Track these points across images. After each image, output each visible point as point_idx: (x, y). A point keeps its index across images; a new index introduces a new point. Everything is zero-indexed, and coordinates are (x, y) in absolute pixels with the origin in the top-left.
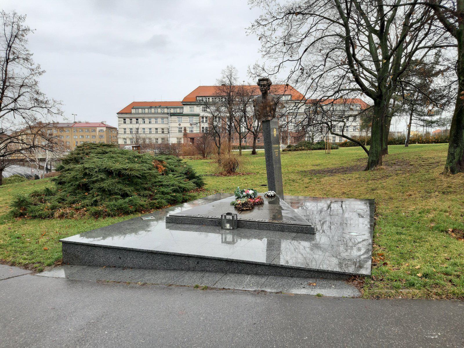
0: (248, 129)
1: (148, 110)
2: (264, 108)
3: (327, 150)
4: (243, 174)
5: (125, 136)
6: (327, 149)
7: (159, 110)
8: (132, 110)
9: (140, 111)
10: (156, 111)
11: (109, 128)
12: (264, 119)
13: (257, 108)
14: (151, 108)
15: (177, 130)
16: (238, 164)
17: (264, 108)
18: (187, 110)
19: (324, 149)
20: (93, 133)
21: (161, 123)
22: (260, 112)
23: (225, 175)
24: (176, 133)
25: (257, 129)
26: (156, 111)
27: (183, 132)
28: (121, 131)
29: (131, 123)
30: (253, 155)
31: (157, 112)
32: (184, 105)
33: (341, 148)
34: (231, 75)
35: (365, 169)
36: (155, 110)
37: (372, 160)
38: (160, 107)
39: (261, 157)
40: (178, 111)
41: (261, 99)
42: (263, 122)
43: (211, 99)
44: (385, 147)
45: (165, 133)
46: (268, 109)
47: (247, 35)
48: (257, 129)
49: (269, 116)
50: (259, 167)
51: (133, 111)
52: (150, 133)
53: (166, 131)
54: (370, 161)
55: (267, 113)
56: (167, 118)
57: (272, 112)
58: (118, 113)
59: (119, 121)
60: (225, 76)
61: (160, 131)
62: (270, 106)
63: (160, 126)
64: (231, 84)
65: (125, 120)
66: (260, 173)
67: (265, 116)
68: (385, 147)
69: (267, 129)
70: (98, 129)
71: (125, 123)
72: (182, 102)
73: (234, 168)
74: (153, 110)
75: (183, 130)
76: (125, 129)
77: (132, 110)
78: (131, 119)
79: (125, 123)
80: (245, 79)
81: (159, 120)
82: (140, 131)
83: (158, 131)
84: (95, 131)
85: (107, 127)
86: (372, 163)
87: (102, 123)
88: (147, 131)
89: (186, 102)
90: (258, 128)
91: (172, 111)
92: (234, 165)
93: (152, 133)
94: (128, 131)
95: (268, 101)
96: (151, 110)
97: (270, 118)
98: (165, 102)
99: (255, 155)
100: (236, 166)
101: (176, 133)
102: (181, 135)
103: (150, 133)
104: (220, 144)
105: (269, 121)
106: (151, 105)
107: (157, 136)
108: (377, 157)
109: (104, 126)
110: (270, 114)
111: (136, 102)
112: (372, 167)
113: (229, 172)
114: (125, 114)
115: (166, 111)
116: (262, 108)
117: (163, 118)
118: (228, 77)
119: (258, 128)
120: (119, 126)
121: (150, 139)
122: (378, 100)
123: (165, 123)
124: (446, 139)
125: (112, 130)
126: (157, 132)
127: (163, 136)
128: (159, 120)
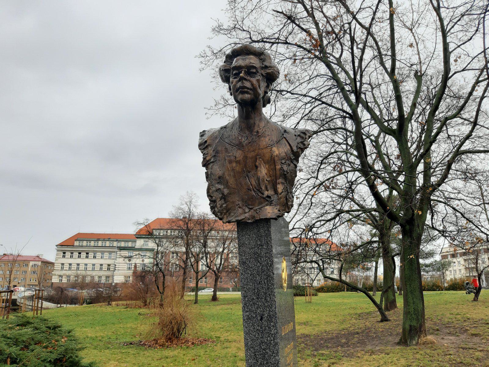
0: (208, 267)
1: (95, 243)
2: (248, 167)
3: (307, 297)
4: (193, 343)
5: (62, 273)
6: (307, 295)
7: (108, 244)
8: (75, 242)
9: (85, 243)
10: (104, 244)
11: (46, 263)
12: (245, 215)
13: (217, 170)
14: (98, 240)
15: (126, 267)
16: (186, 325)
17: (248, 167)
18: (140, 243)
19: (304, 295)
20: (24, 268)
21: (108, 258)
22: (232, 181)
23: (162, 346)
24: (125, 270)
25: (219, 267)
26: (104, 244)
27: (133, 269)
28: (58, 266)
29: (79, 257)
30: (213, 303)
31: (105, 245)
32: (137, 238)
33: (321, 294)
34: (191, 202)
35: (397, 340)
36: (103, 243)
37: (410, 326)
38: (109, 240)
39: (224, 306)
40: (130, 244)
41: (235, 132)
42: (241, 225)
43: (169, 231)
44: (393, 298)
45: (111, 269)
46: (263, 171)
47: (208, 118)
48: (219, 267)
49: (268, 200)
50: (220, 326)
51: (76, 243)
52: (93, 269)
53: (112, 268)
54: (407, 327)
55: (260, 190)
56: (116, 252)
57: (280, 188)
58: (57, 246)
59: (57, 255)
60: (184, 202)
61: (105, 267)
62: (272, 161)
63: (105, 262)
64: (190, 212)
65: (64, 253)
66: (222, 339)
67: (249, 202)
68: (393, 298)
69: (257, 257)
70: (31, 263)
71: (64, 257)
72: (136, 235)
73: (179, 331)
74: (100, 243)
75: (133, 266)
76: (63, 264)
77: (75, 242)
78: (72, 253)
79: (64, 257)
80: (199, 157)
81: (106, 255)
82: (82, 267)
83: (103, 267)
84: (27, 265)
85: (42, 262)
86: (410, 330)
87: (37, 256)
88: (90, 267)
89: (139, 236)
90: (220, 266)
91: (123, 244)
92: (179, 325)
93: (96, 269)
94: (66, 267)
95: (265, 141)
96: (98, 243)
97: (270, 211)
98: (116, 234)
99: (216, 303)
100: (183, 326)
101: (125, 270)
102: (130, 273)
103: (93, 269)
104: (164, 288)
105: (267, 221)
106: (98, 237)
107: (101, 273)
108: (418, 320)
109: (39, 260)
110: (270, 192)
111: (81, 233)
112: (412, 338)
113: (170, 339)
114: (66, 247)
115: (115, 244)
116: (238, 168)
117: (110, 253)
118: (186, 204)
119: (220, 266)
120: (56, 260)
121: (93, 277)
122: (408, 227)
123: (112, 258)
124: (433, 286)
125: (48, 265)
126: (101, 269)
127: (108, 273)
128: (106, 255)
